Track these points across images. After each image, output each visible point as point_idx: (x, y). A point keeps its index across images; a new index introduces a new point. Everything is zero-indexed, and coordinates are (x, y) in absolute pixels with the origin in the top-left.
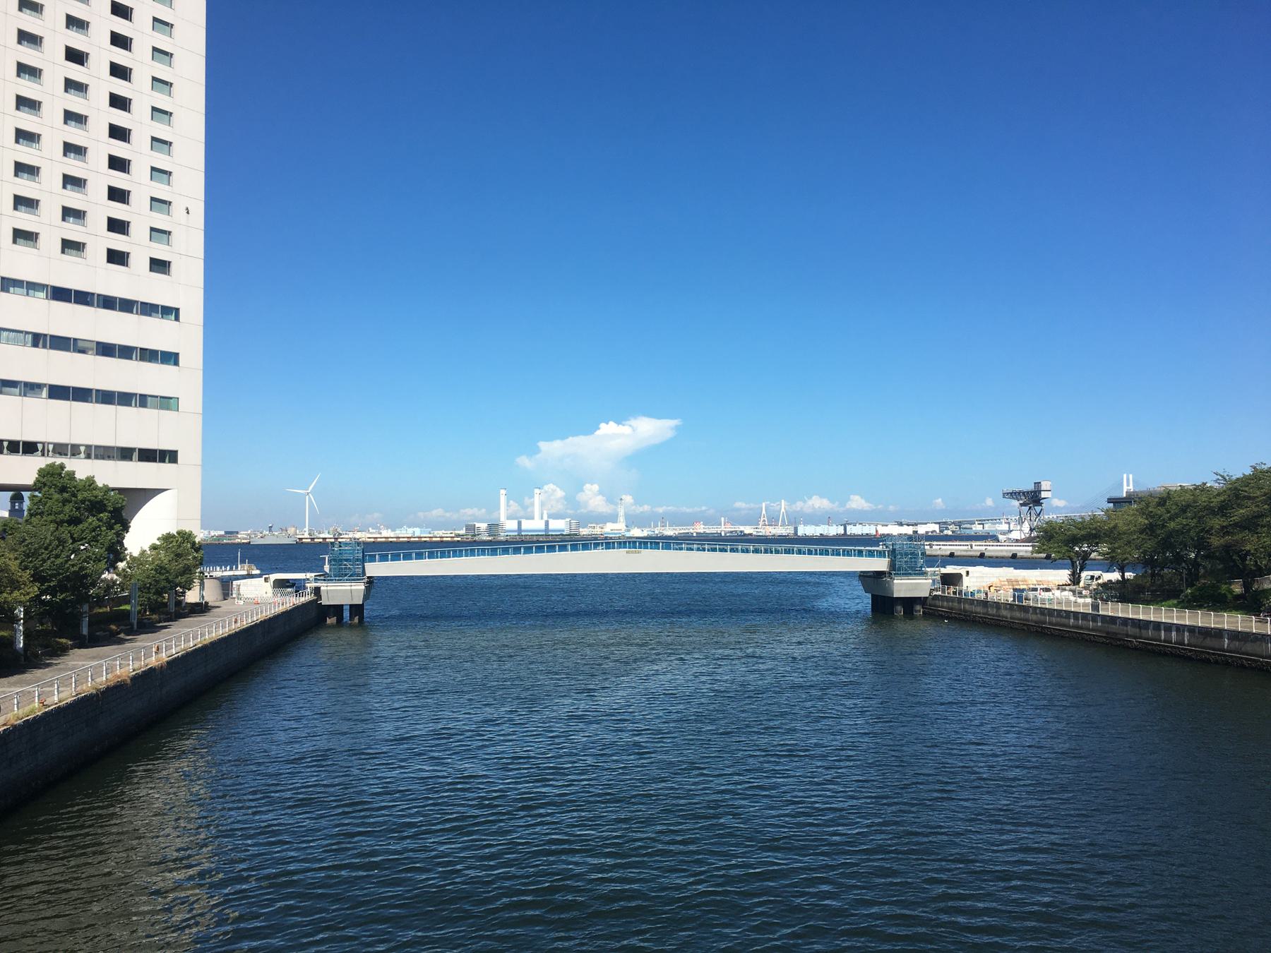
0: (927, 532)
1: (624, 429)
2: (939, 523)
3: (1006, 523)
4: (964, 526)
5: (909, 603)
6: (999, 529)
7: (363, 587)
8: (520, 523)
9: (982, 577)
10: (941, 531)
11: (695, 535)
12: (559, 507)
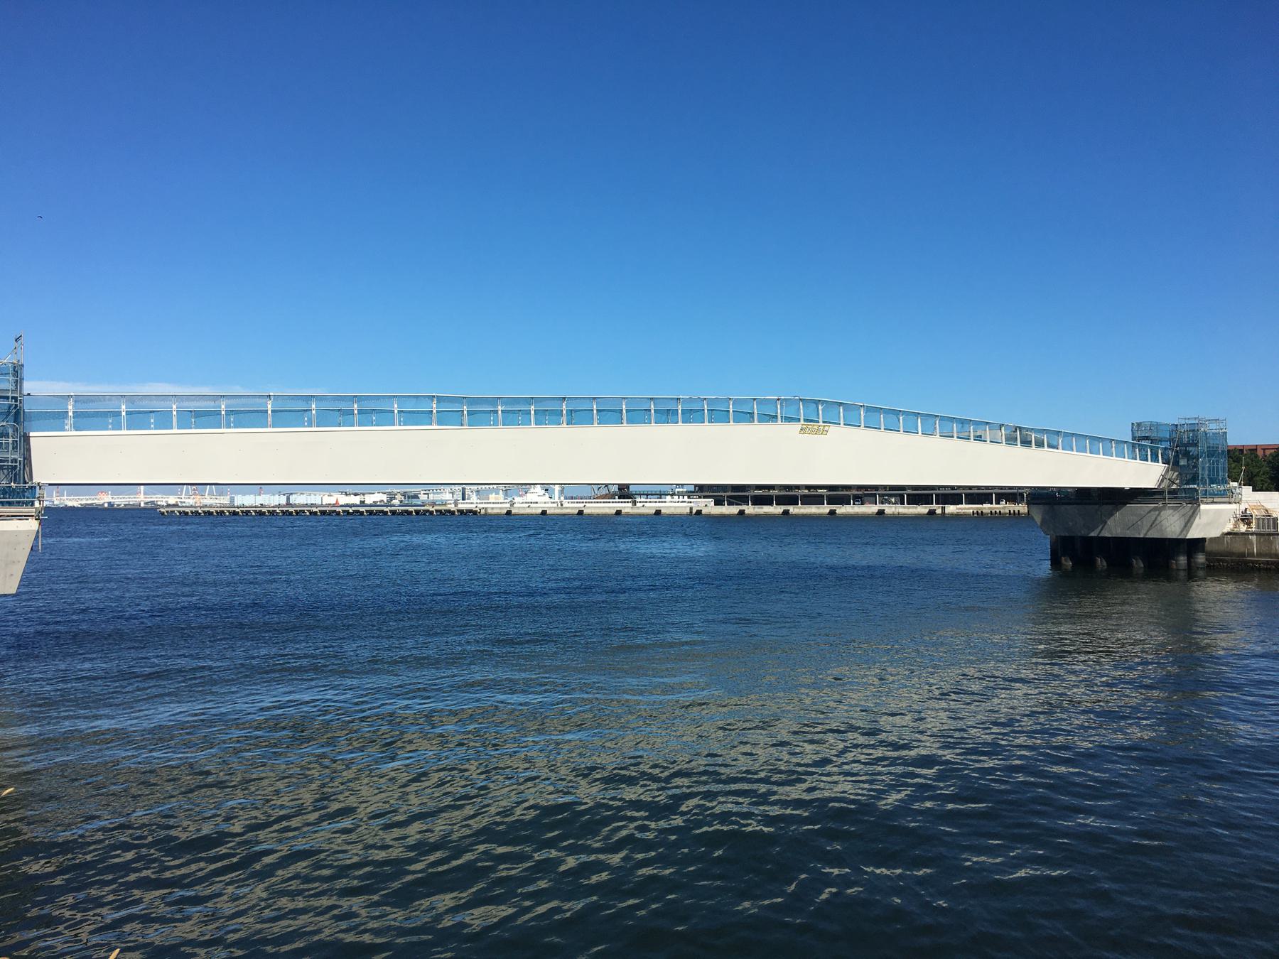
11: (106, 505)
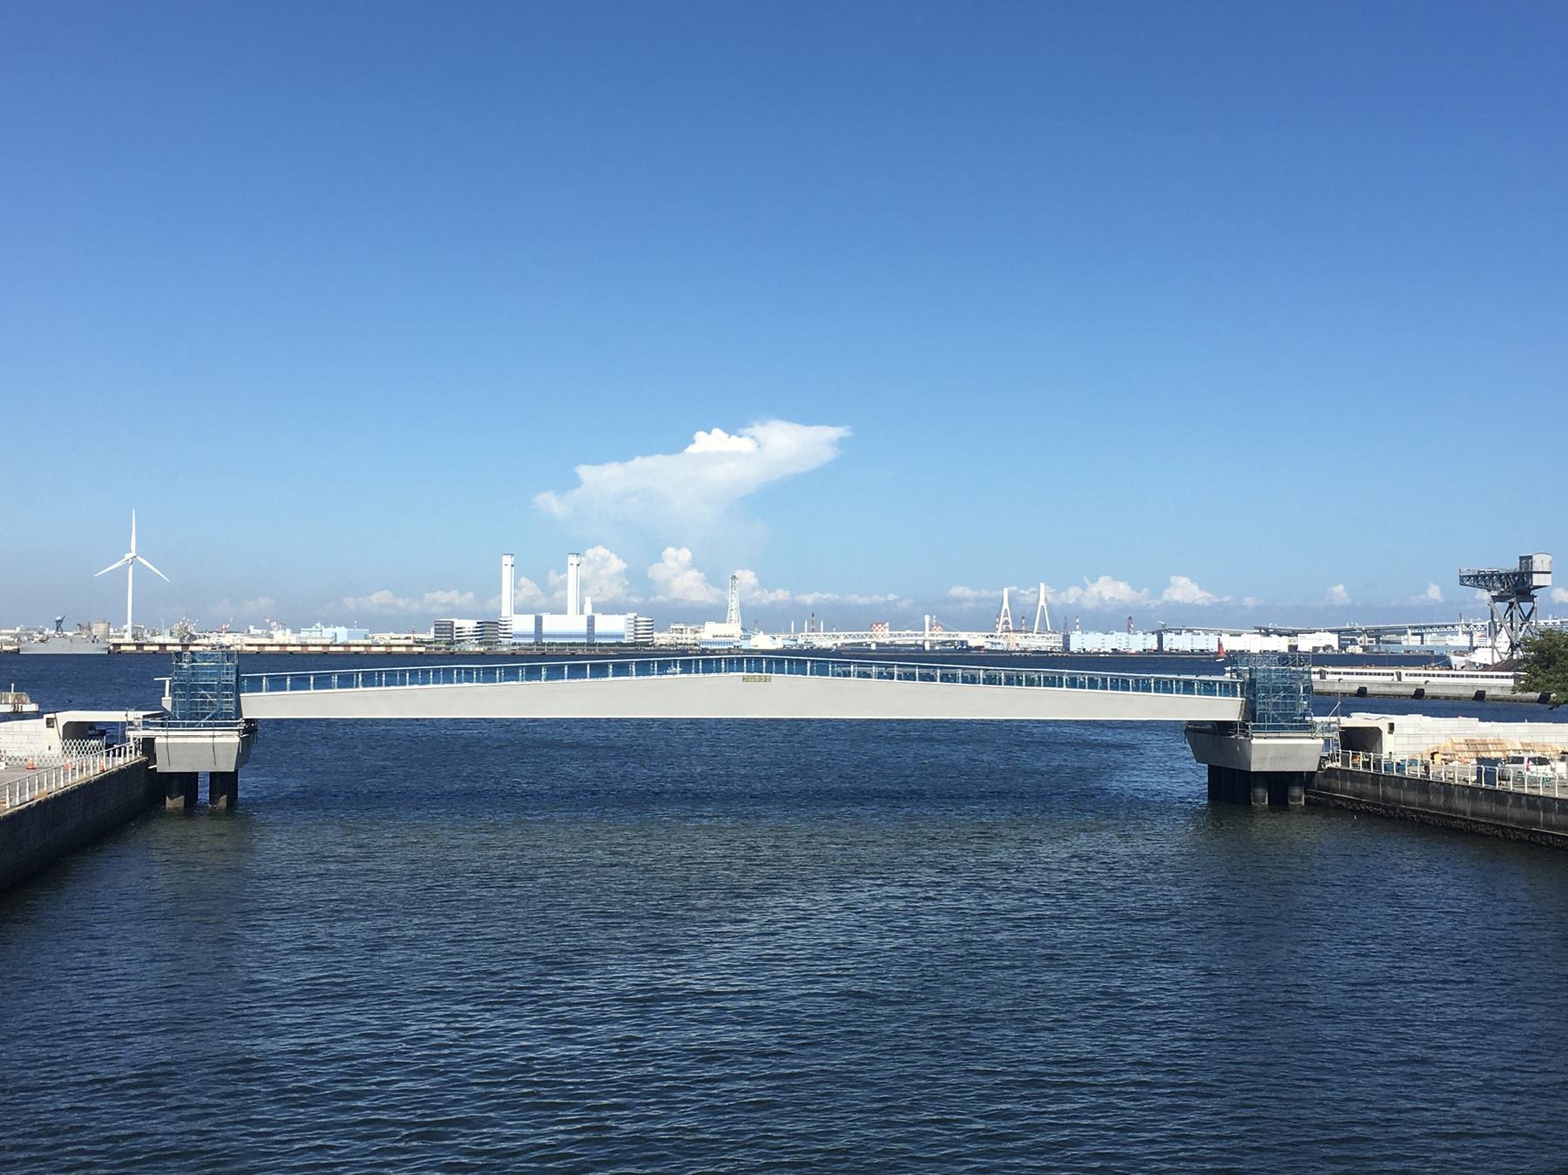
0: (1316, 649)
2: (1338, 632)
3: (1464, 633)
4: (1387, 638)
5: (1280, 783)
7: (237, 740)
8: (539, 622)
10: (1343, 647)
11: (873, 647)
12: (614, 591)
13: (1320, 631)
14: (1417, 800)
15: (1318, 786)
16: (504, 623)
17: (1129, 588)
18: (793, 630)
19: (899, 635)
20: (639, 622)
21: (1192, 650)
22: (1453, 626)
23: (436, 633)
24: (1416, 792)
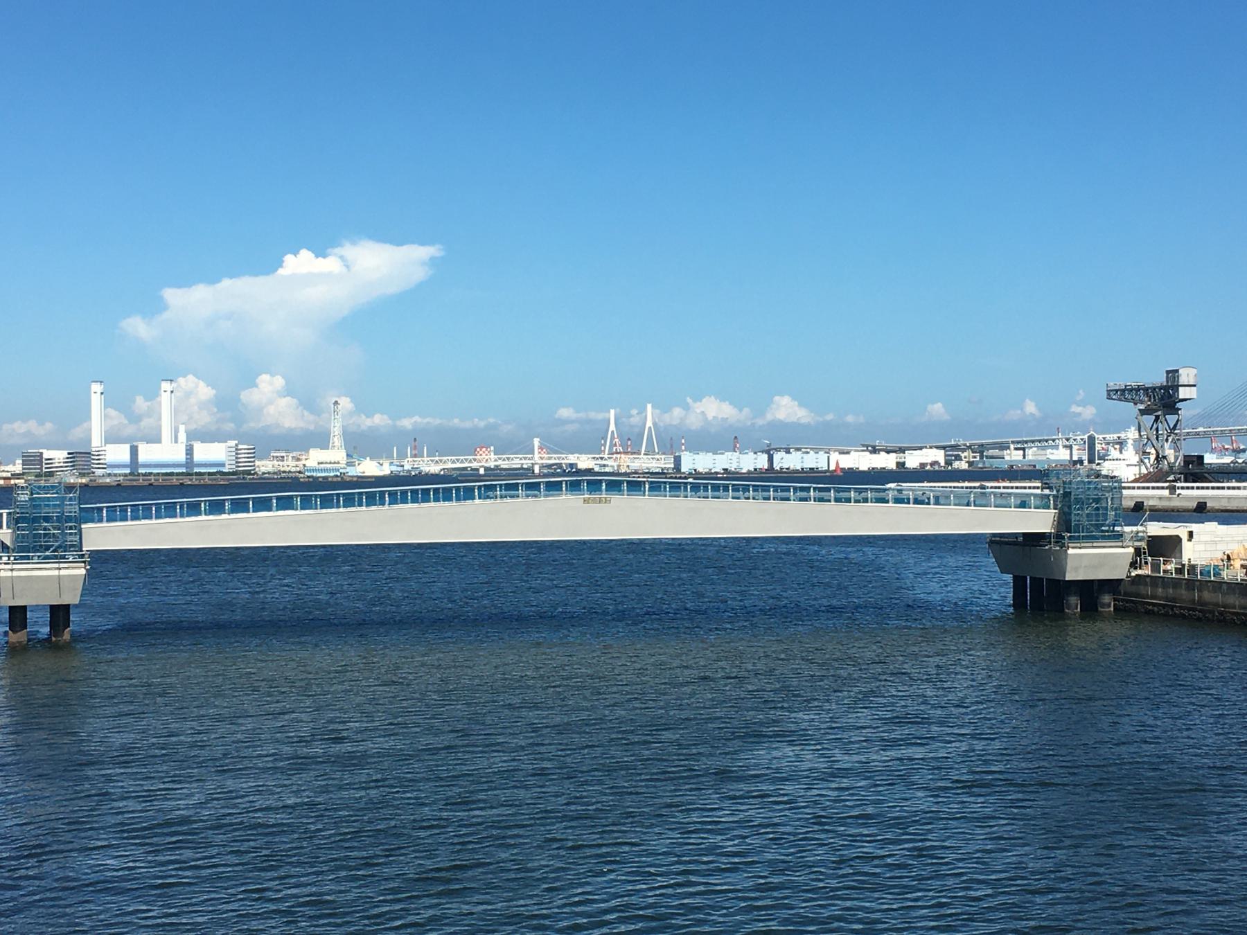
0: (923, 465)
1: (330, 264)
2: (943, 448)
3: (1065, 446)
4: (991, 452)
5: (1091, 590)
6: (1052, 457)
7: (83, 572)
8: (134, 451)
9: (1215, 543)
10: (948, 463)
11: (482, 471)
12: (204, 419)
13: (926, 447)
14: (1237, 603)
15: (1125, 593)
16: (97, 453)
17: (731, 407)
18: (395, 456)
19: (508, 459)
20: (241, 449)
21: (802, 469)
22: (1054, 440)
23: (23, 465)
24: (1237, 595)
